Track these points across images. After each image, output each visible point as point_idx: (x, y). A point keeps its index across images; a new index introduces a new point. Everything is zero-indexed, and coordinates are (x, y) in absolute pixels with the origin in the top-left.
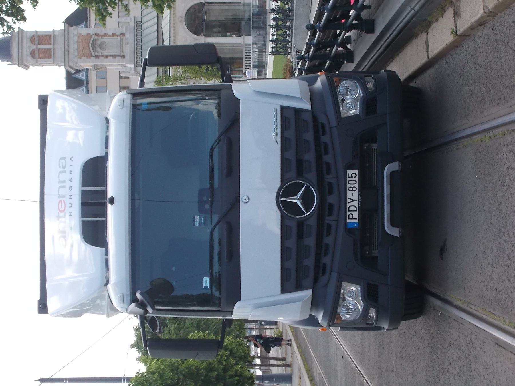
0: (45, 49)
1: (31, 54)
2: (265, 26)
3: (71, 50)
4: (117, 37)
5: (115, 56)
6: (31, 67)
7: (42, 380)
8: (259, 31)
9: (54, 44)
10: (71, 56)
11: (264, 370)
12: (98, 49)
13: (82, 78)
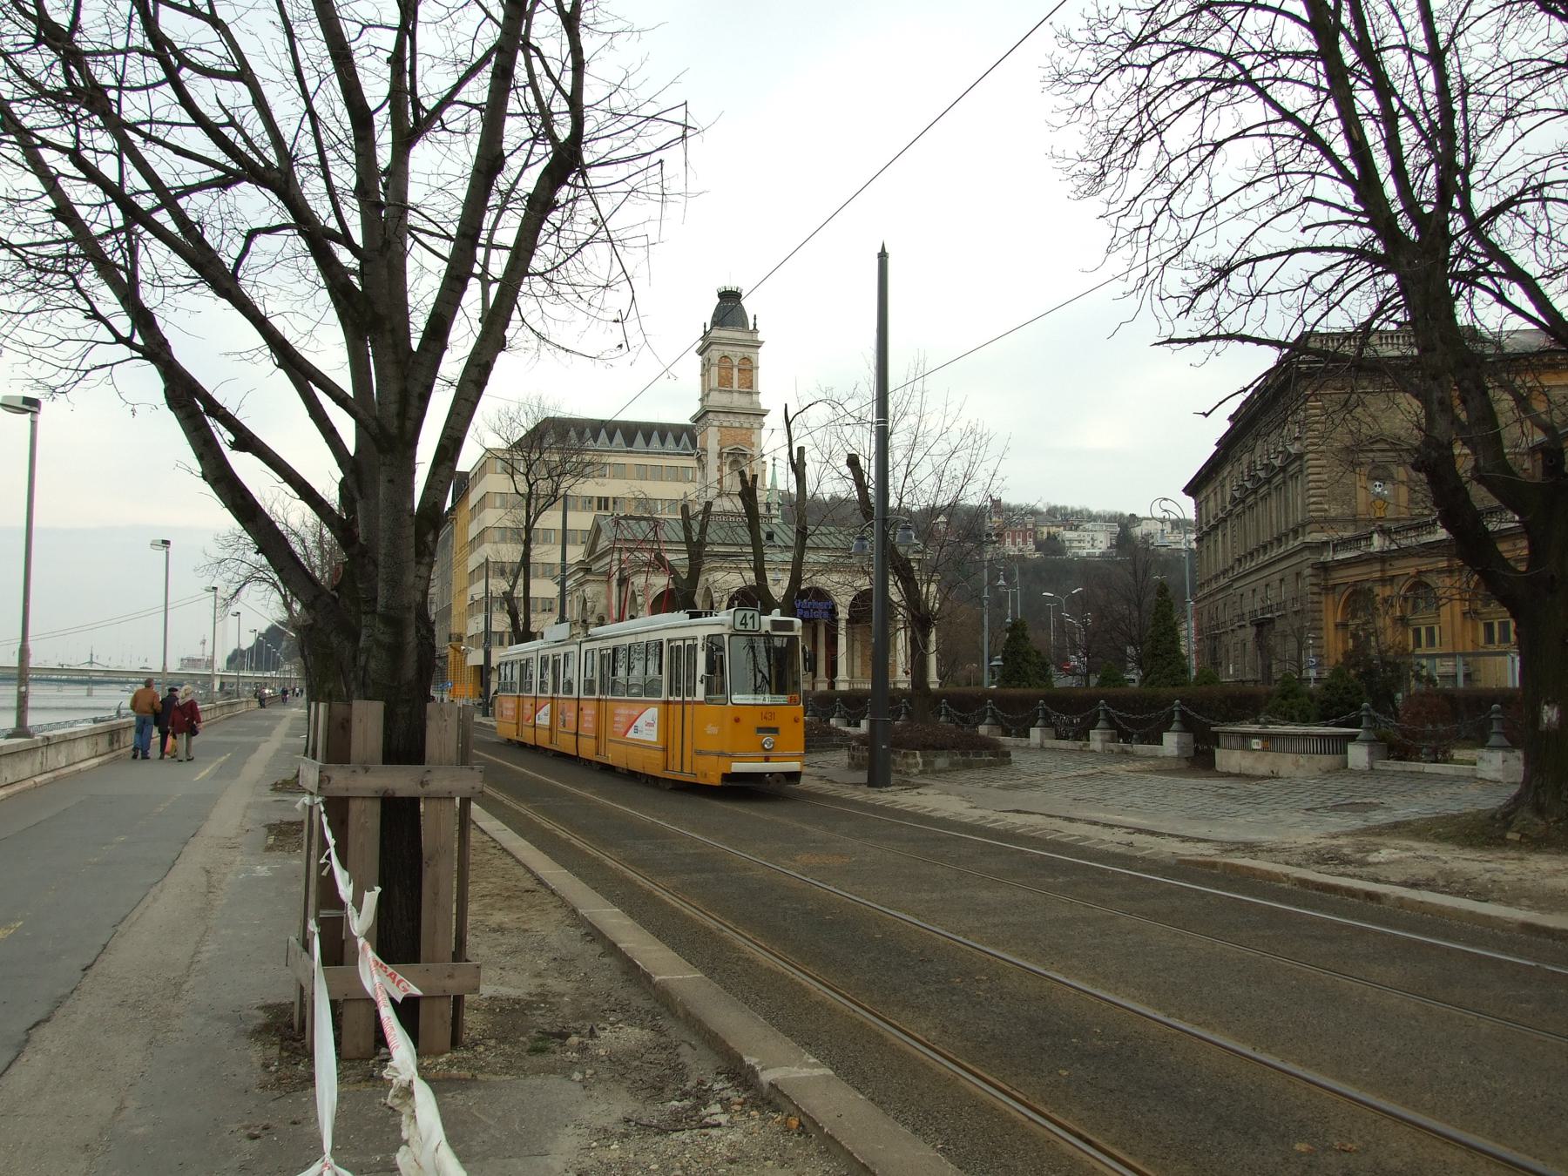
1: (725, 357)
3: (731, 417)
6: (700, 358)
7: (883, 256)
9: (740, 392)
10: (722, 416)
12: (731, 459)
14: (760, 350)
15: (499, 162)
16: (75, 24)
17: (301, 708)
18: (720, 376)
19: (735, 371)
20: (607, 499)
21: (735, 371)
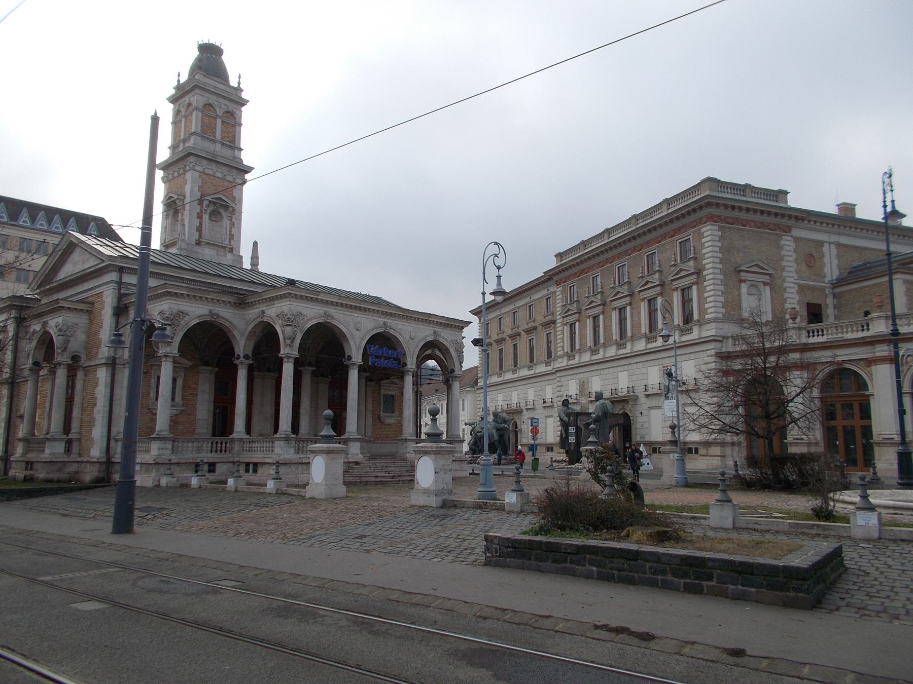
0: (215, 128)
2: (824, 517)
3: (213, 166)
4: (227, 240)
5: (199, 229)
6: (172, 106)
8: (569, 492)
10: (204, 162)
11: (224, 84)
12: (211, 208)
13: (22, 221)
14: (243, 109)
17: (701, 236)
21: (219, 121)
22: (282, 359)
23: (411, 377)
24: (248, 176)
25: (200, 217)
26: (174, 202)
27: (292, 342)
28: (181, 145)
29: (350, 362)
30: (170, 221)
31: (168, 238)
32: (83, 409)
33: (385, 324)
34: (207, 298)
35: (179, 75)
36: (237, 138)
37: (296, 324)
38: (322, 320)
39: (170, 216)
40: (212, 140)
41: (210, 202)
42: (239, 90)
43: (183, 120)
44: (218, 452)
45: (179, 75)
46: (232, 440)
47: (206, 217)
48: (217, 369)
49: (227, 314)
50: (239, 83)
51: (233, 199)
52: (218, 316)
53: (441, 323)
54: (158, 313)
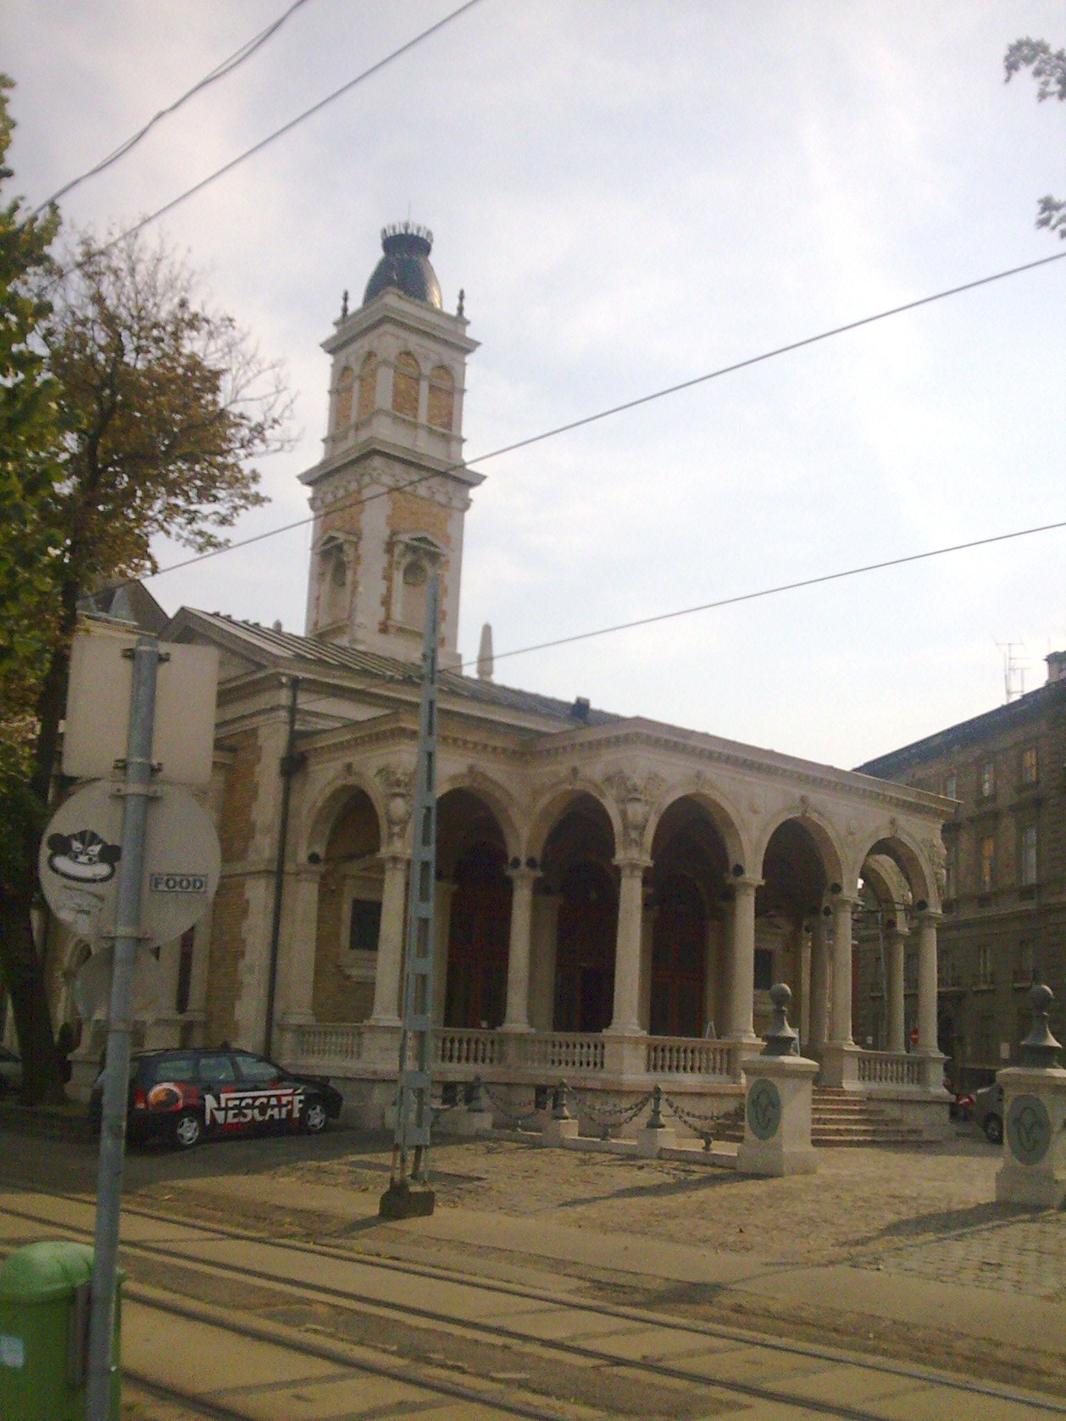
0: (417, 400)
6: (329, 359)
10: (398, 469)
12: (408, 559)
15: (906, 755)
16: (387, 486)
18: (397, 392)
19: (424, 386)
20: (814, 1132)
21: (424, 386)
22: (618, 870)
23: (849, 915)
24: (473, 493)
25: (388, 578)
26: (340, 548)
27: (642, 835)
28: (352, 433)
29: (740, 879)
30: (326, 586)
31: (325, 621)
32: (214, 964)
33: (803, 800)
34: (465, 742)
35: (346, 299)
36: (454, 418)
37: (648, 797)
38: (465, 783)
39: (328, 578)
40: (410, 423)
41: (408, 547)
42: (460, 319)
43: (356, 386)
44: (455, 1060)
45: (346, 299)
46: (503, 1040)
47: (398, 577)
48: (456, 887)
49: (497, 771)
50: (461, 309)
51: (447, 538)
52: (486, 778)
53: (905, 801)
54: (375, 772)
